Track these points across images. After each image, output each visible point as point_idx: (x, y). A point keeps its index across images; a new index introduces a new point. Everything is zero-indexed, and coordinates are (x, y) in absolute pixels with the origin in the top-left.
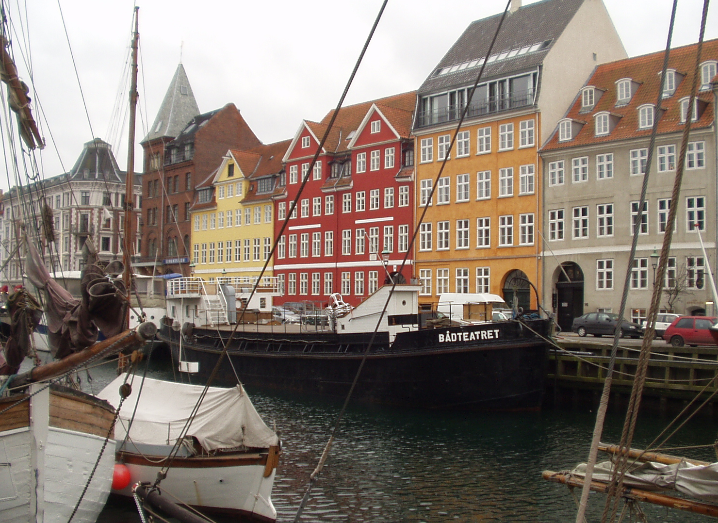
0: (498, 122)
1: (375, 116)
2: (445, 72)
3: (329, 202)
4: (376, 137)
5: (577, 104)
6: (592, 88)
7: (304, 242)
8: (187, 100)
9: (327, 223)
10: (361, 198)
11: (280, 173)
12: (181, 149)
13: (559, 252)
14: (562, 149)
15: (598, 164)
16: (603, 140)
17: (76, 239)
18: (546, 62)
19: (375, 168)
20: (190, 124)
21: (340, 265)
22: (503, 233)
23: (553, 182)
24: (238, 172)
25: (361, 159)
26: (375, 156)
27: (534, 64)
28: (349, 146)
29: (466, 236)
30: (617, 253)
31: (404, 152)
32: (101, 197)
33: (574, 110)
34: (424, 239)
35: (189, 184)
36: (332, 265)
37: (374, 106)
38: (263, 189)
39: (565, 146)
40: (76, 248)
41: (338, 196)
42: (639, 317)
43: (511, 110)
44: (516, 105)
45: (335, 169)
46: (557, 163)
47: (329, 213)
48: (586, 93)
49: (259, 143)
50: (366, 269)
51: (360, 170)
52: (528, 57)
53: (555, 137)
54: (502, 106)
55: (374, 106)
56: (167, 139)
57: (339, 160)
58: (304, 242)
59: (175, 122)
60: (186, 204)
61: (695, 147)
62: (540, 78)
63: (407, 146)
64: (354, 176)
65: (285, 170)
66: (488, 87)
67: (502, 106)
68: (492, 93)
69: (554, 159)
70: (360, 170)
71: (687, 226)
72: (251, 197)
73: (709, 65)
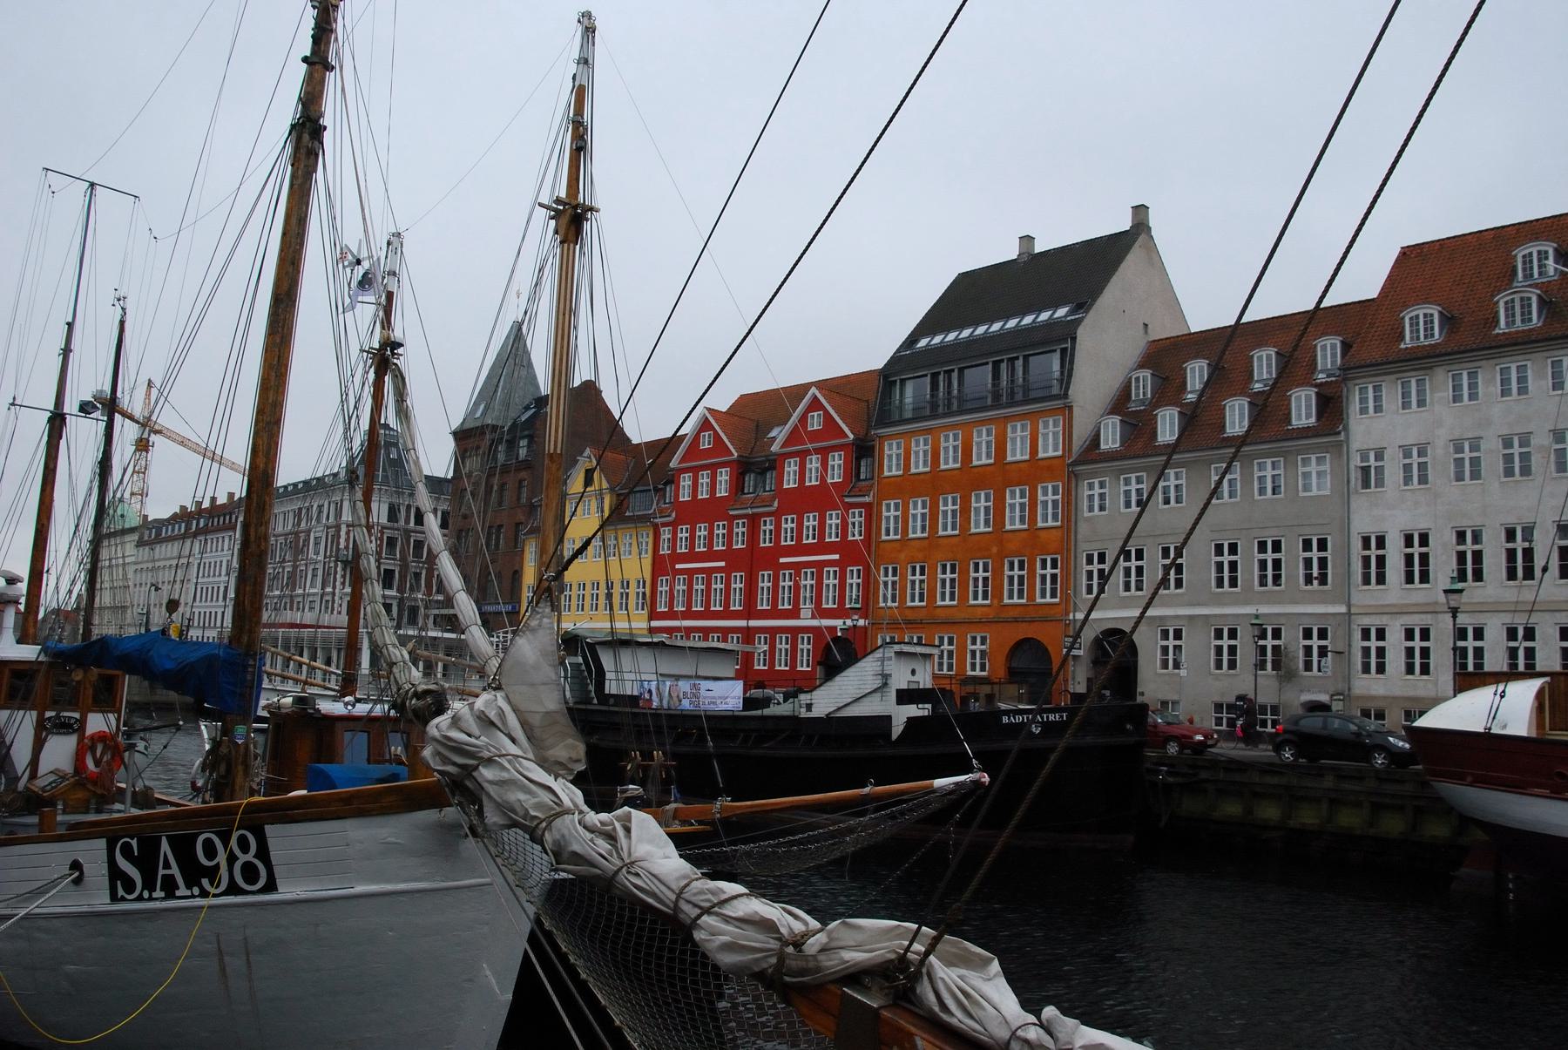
0: (1007, 419)
1: (815, 405)
2: (923, 343)
3: (740, 529)
4: (707, 453)
5: (1124, 395)
6: (1147, 373)
7: (699, 587)
8: (524, 373)
9: (734, 560)
10: (790, 525)
11: (666, 484)
12: (512, 445)
13: (1114, 612)
14: (1101, 461)
15: (1123, 488)
16: (1305, 433)
17: (344, 569)
18: (1080, 332)
19: (703, 495)
20: (527, 408)
21: (753, 623)
22: (943, 585)
23: (1091, 509)
24: (600, 481)
25: (791, 467)
26: (704, 479)
27: (1062, 339)
28: (775, 448)
29: (952, 587)
30: (1191, 618)
31: (858, 460)
32: (385, 508)
33: (1120, 404)
34: (976, 586)
35: (524, 495)
36: (742, 623)
37: (813, 390)
38: (635, 507)
39: (1112, 456)
40: (343, 584)
41: (754, 522)
42: (441, 655)
43: (961, 412)
44: (1033, 395)
45: (750, 480)
46: (1096, 481)
47: (855, 535)
48: (1137, 379)
49: (629, 440)
50: (795, 631)
51: (790, 483)
52: (1051, 324)
53: (1095, 440)
54: (1012, 394)
55: (813, 390)
56: (494, 428)
57: (754, 466)
58: (699, 587)
59: (507, 405)
60: (518, 524)
61: (1172, 476)
62: (1072, 355)
63: (863, 450)
64: (780, 492)
65: (673, 480)
66: (928, 379)
67: (1012, 394)
68: (996, 375)
69: (1094, 475)
70: (790, 483)
71: (1302, 580)
72: (616, 518)
73: (1328, 343)
